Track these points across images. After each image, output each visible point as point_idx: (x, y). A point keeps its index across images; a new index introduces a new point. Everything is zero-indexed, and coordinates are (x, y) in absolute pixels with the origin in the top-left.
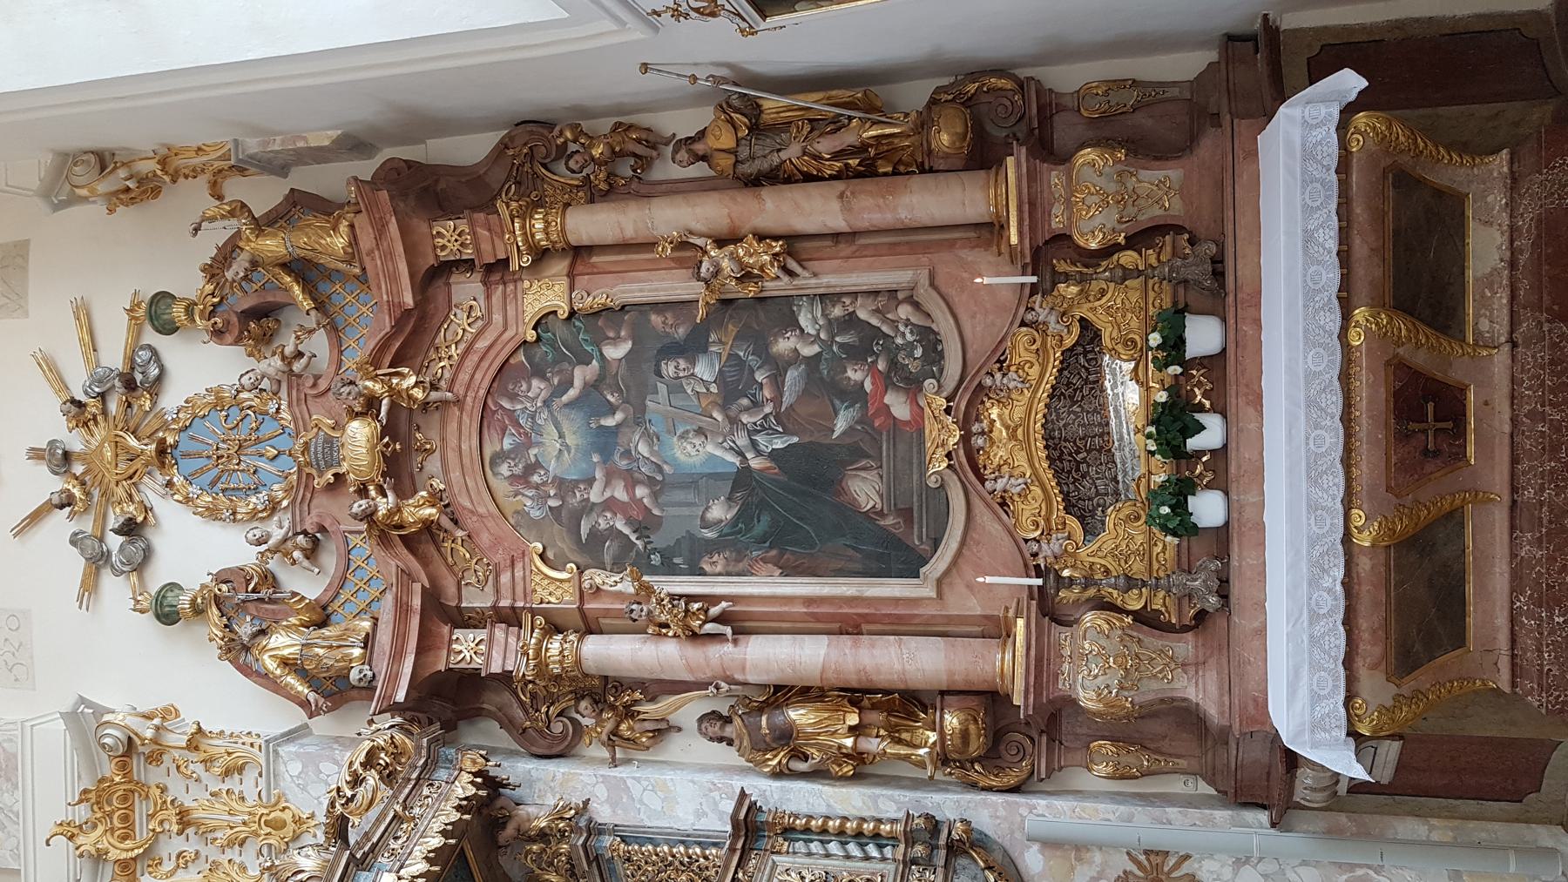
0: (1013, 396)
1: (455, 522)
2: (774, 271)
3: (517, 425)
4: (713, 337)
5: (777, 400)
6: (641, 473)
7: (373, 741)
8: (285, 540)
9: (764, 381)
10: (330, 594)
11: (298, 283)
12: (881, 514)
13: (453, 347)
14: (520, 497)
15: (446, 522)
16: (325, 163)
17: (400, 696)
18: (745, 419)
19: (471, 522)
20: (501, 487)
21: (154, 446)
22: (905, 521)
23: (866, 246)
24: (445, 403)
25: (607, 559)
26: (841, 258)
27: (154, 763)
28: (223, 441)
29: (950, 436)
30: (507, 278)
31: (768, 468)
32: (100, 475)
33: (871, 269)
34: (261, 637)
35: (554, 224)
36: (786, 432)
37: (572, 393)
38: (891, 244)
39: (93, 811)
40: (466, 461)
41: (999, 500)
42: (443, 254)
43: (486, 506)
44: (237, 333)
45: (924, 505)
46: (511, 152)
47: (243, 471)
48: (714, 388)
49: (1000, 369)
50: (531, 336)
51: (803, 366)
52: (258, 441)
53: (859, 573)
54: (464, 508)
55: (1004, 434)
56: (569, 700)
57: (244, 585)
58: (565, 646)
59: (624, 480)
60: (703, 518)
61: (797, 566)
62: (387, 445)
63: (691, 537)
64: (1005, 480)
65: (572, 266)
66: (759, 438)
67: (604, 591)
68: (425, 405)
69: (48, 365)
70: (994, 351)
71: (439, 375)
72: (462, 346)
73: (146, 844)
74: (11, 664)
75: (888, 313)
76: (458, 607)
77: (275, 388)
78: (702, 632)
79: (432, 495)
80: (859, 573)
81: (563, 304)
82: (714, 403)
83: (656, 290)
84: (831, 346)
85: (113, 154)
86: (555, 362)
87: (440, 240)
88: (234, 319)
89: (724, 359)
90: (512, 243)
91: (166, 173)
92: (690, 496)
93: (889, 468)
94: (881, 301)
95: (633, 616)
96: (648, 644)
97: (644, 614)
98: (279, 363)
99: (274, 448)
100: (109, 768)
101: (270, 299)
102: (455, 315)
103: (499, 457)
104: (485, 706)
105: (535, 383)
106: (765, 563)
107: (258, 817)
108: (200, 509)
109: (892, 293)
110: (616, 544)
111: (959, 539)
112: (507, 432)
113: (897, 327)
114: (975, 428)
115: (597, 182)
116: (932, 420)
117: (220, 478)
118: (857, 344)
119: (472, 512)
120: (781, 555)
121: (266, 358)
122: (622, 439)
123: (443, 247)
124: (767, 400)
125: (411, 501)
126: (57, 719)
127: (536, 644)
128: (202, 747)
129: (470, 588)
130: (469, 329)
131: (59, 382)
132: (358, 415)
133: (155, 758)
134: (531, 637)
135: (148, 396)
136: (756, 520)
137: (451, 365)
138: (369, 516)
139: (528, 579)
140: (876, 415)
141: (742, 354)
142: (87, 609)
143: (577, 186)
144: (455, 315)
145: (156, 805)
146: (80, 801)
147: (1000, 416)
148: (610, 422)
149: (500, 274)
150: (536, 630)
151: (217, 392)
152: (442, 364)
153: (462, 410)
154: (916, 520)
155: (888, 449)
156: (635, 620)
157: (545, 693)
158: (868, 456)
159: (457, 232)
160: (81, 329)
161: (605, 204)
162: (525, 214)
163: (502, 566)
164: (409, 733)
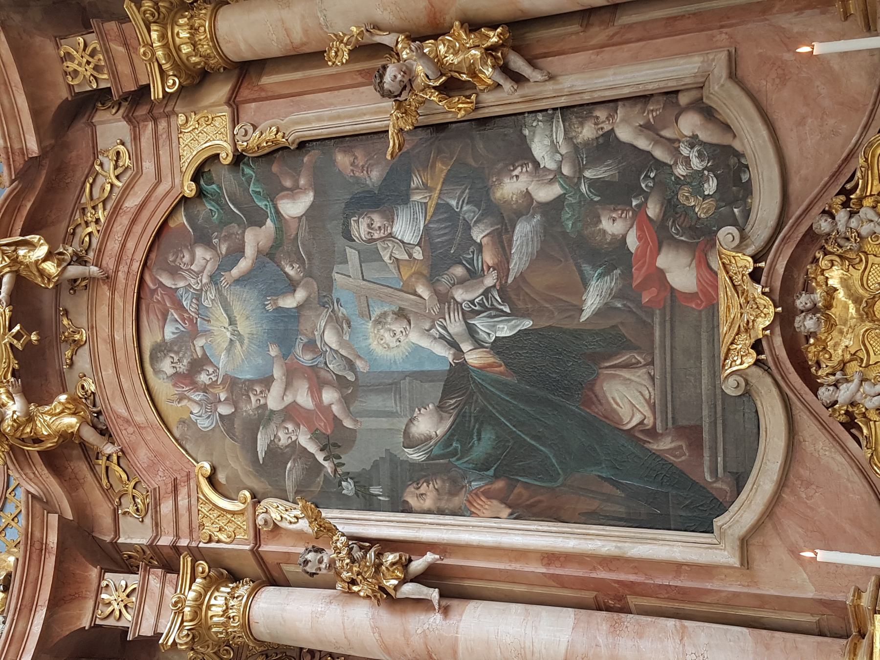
0: (868, 248)
1: (105, 433)
2: (488, 72)
3: (180, 307)
4: (416, 182)
5: (502, 267)
6: (329, 371)
9: (485, 241)
12: (652, 433)
13: (100, 206)
14: (185, 402)
15: (89, 435)
18: (460, 295)
19: (125, 434)
20: (163, 388)
22: (690, 445)
23: (630, 27)
25: (290, 485)
26: (593, 48)
29: (757, 317)
31: (490, 365)
33: (636, 59)
36: (516, 313)
37: (244, 265)
38: (668, 19)
40: (120, 355)
41: (843, 418)
42: (76, 82)
43: (145, 414)
45: (719, 422)
48: (418, 254)
49: (845, 205)
50: (189, 189)
51: (538, 217)
53: (621, 519)
54: (119, 416)
55: (852, 310)
59: (309, 379)
60: (406, 433)
61: (532, 505)
62: (18, 336)
63: (393, 460)
64: (853, 386)
66: (479, 323)
67: (286, 530)
70: (835, 175)
71: (86, 244)
75: (665, 128)
76: (114, 544)
78: (399, 596)
79: (73, 400)
80: (621, 519)
81: (225, 144)
82: (419, 274)
83: (338, 117)
84: (578, 184)
86: (223, 223)
87: (69, 64)
89: (431, 211)
90: (150, 60)
92: (389, 403)
93: (664, 365)
94: (655, 108)
95: (308, 569)
96: (333, 606)
97: (323, 566)
102: (101, 165)
103: (162, 349)
105: (200, 253)
106: (488, 498)
109: (672, 94)
110: (299, 465)
111: (775, 477)
113: (677, 149)
114: (802, 301)
116: (730, 291)
118: (616, 179)
119: (127, 421)
120: (511, 487)
122: (305, 326)
124: (489, 268)
125: (47, 408)
127: (196, 600)
129: (129, 518)
134: (190, 588)
136: (475, 438)
137: (98, 231)
139: (194, 510)
140: (643, 285)
141: (453, 203)
144: (101, 165)
147: (844, 282)
148: (289, 302)
150: (198, 580)
152: (89, 230)
153: (113, 291)
154: (706, 444)
155: (663, 337)
156: (312, 574)
158: (636, 348)
159: (89, 50)
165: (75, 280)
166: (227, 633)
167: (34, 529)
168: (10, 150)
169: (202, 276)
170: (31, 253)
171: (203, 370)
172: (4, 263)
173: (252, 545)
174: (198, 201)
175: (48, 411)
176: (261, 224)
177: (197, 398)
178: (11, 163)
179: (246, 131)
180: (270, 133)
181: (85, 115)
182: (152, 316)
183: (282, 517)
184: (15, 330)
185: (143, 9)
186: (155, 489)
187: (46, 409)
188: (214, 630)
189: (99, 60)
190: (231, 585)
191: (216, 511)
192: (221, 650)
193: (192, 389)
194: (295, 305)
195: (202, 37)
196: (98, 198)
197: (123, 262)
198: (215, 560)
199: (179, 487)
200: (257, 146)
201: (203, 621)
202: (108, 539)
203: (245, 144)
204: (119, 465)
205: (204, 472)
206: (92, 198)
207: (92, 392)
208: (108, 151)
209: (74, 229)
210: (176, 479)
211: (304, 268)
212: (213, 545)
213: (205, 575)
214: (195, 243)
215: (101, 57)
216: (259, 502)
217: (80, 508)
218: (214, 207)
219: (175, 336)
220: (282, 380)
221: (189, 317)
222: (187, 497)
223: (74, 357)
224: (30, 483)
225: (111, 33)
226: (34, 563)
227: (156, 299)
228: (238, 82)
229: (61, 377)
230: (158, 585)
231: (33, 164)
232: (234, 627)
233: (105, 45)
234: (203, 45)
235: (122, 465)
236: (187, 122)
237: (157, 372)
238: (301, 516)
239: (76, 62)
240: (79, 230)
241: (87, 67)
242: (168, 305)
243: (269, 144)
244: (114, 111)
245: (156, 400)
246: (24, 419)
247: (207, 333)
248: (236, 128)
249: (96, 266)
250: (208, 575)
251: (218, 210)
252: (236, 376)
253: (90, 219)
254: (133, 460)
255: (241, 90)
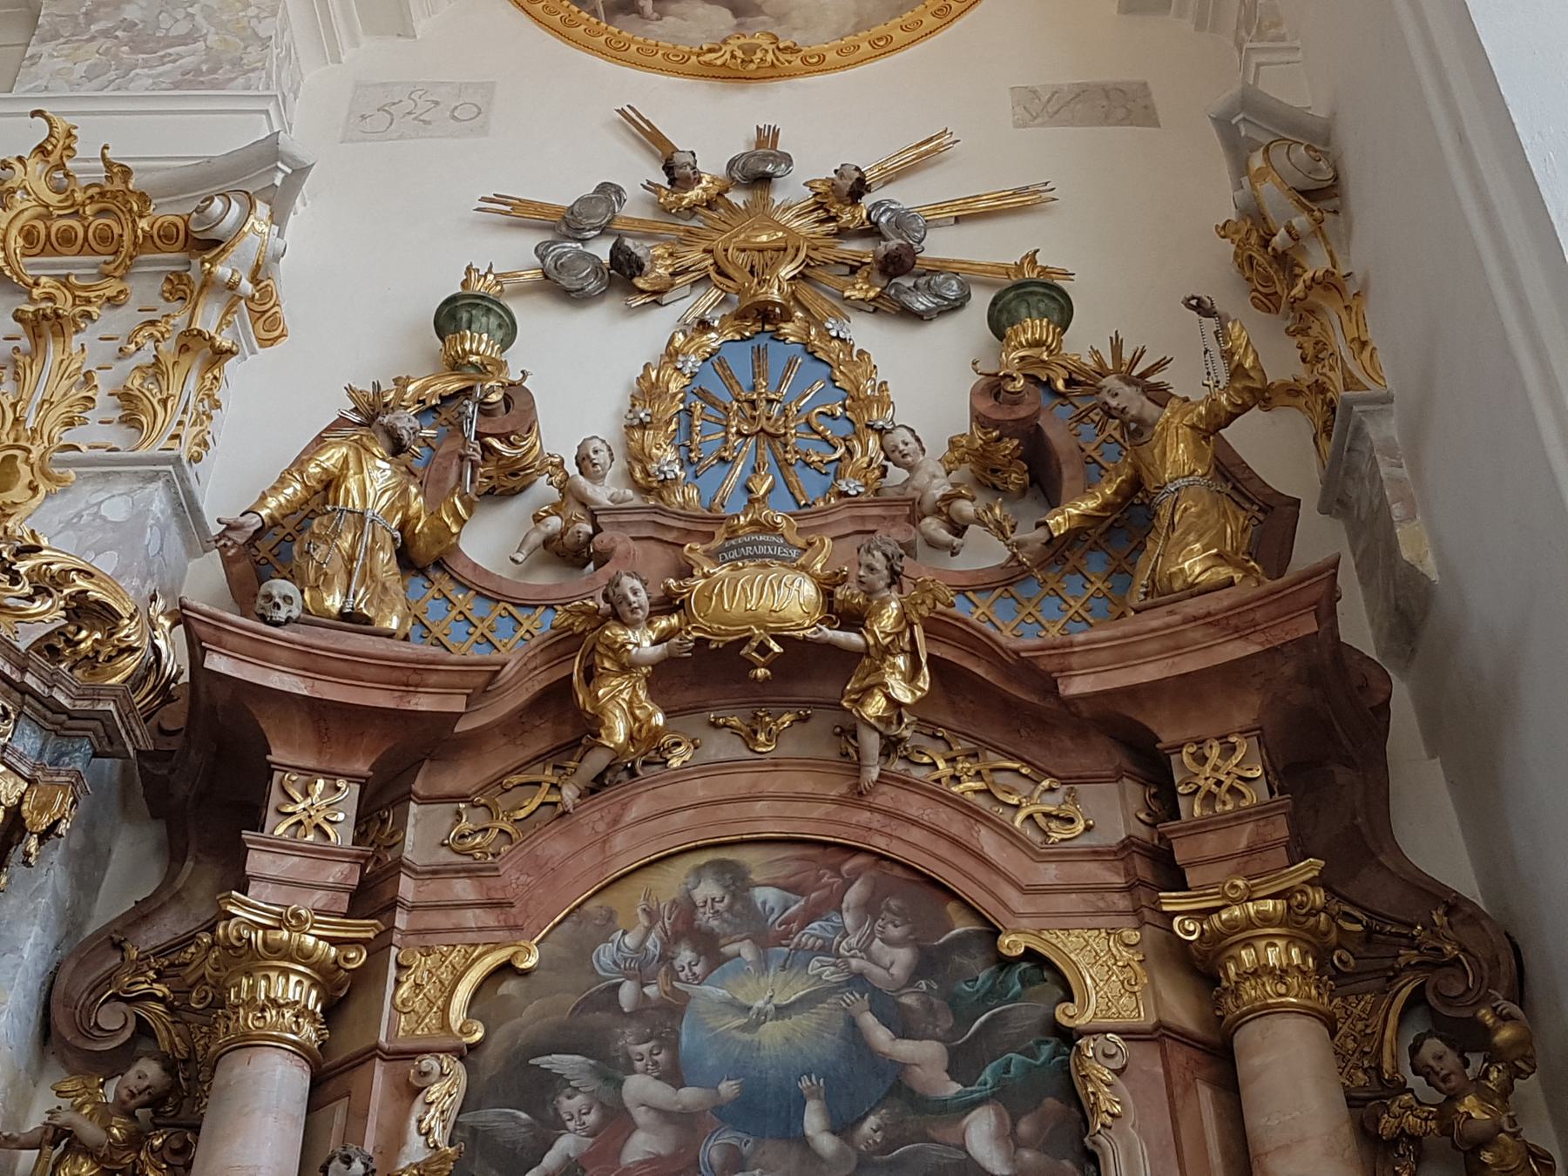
1: (597, 786)
3: (809, 916)
7: (132, 617)
8: (583, 503)
10: (468, 574)
11: (1103, 507)
13: (979, 785)
14: (644, 921)
15: (596, 762)
16: (1360, 578)
17: (217, 663)
19: (594, 818)
20: (670, 883)
21: (776, 297)
24: (858, 768)
25: (489, 1116)
27: (167, 287)
28: (783, 411)
30: (1142, 892)
32: (726, 227)
34: (388, 443)
35: (1282, 989)
37: (881, 1036)
39: (90, 186)
40: (728, 811)
43: (626, 851)
44: (995, 417)
46: (1438, 917)
47: (726, 440)
50: (1012, 944)
52: (783, 465)
54: (625, 806)
56: (172, 1044)
57: (500, 431)
58: (288, 1014)
59: (674, 1157)
62: (763, 649)
65: (1182, 1037)
68: (849, 731)
69: (927, 152)
71: (916, 758)
72: (982, 802)
73: (12, 270)
74: (392, 109)
76: (408, 796)
77: (890, 494)
79: (656, 733)
81: (1090, 1013)
85: (1336, 212)
86: (953, 1001)
87: (1216, 751)
88: (1022, 412)
90: (1225, 896)
91: (1308, 288)
95: (336, 1163)
98: (938, 493)
99: (769, 491)
100: (165, 213)
101: (1067, 472)
102: (1051, 790)
103: (737, 881)
104: (189, 864)
105: (902, 958)
107: (28, 445)
108: (654, 375)
112: (793, 897)
115: (1395, 1109)
117: (713, 405)
119: (616, 821)
121: (948, 473)
123: (1201, 759)
125: (642, 694)
126: (271, 127)
127: (300, 948)
128: (185, 360)
129: (450, 821)
130: (1021, 816)
131: (894, 176)
132: (828, 595)
133: (179, 289)
134: (320, 938)
135: (872, 294)
137: (938, 781)
138: (618, 613)
142: (478, 209)
143: (1378, 1069)
144: (1051, 790)
145: (85, 288)
146: (108, 165)
148: (813, 1121)
149: (1149, 879)
150: (333, 951)
151: (882, 399)
152: (941, 764)
153: (840, 801)
157: (190, 981)
160: (998, 199)
161: (1346, 1130)
162: (1295, 924)
163: (491, 882)
164: (136, 681)
165: (855, 737)
166: (237, 1007)
167: (442, 674)
168: (1067, 650)
169: (862, 958)
170: (898, 677)
171: (699, 955)
172: (880, 636)
173: (386, 1046)
174: (992, 956)
175: (637, 696)
176: (953, 1072)
177: (649, 944)
178: (1047, 652)
179: (1112, 1056)
180: (1109, 1100)
181: (1135, 765)
182: (794, 866)
183: (432, 1103)
184: (773, 644)
185: (1309, 890)
186: (497, 869)
187: (640, 692)
188: (244, 981)
189: (1224, 803)
190: (318, 1009)
191: (450, 977)
192: (207, 988)
193: (666, 933)
194: (809, 1132)
195: (1268, 989)
196: (993, 782)
197: (887, 821)
198: (367, 979)
199: (498, 911)
200: (1087, 1075)
201: (262, 963)
202: (418, 786)
203: (1090, 1054)
204: (543, 804)
205: (520, 956)
206: (993, 770)
207: (667, 761)
208: (1075, 801)
209: (942, 738)
210: (511, 905)
211: (874, 1153)
212: (392, 972)
213: (342, 962)
214: (918, 946)
215: (1229, 807)
216: (461, 1059)
217: (473, 742)
218: (984, 983)
219: (759, 905)
220: (677, 1103)
221: (790, 933)
222: (480, 925)
223: (729, 730)
224: (520, 664)
225: (1270, 827)
226: (385, 674)
227: (824, 875)
228: (1198, 1042)
229: (696, 708)
230: (331, 880)
231: (1049, 686)
232: (246, 1020)
233: (1250, 815)
234: (1255, 988)
235: (543, 809)
236: (1127, 945)
237: (698, 872)
238: (430, 1140)
239: (1220, 762)
240: (941, 746)
241: (1211, 781)
242: (813, 895)
243: (1092, 1098)
244: (1142, 816)
245: (652, 869)
246: (624, 660)
247: (763, 964)
248: (1116, 1038)
249: (880, 775)
250: (340, 968)
251: (978, 991)
252: (686, 1016)
253: (960, 766)
254: (549, 831)
255: (1186, 1048)
